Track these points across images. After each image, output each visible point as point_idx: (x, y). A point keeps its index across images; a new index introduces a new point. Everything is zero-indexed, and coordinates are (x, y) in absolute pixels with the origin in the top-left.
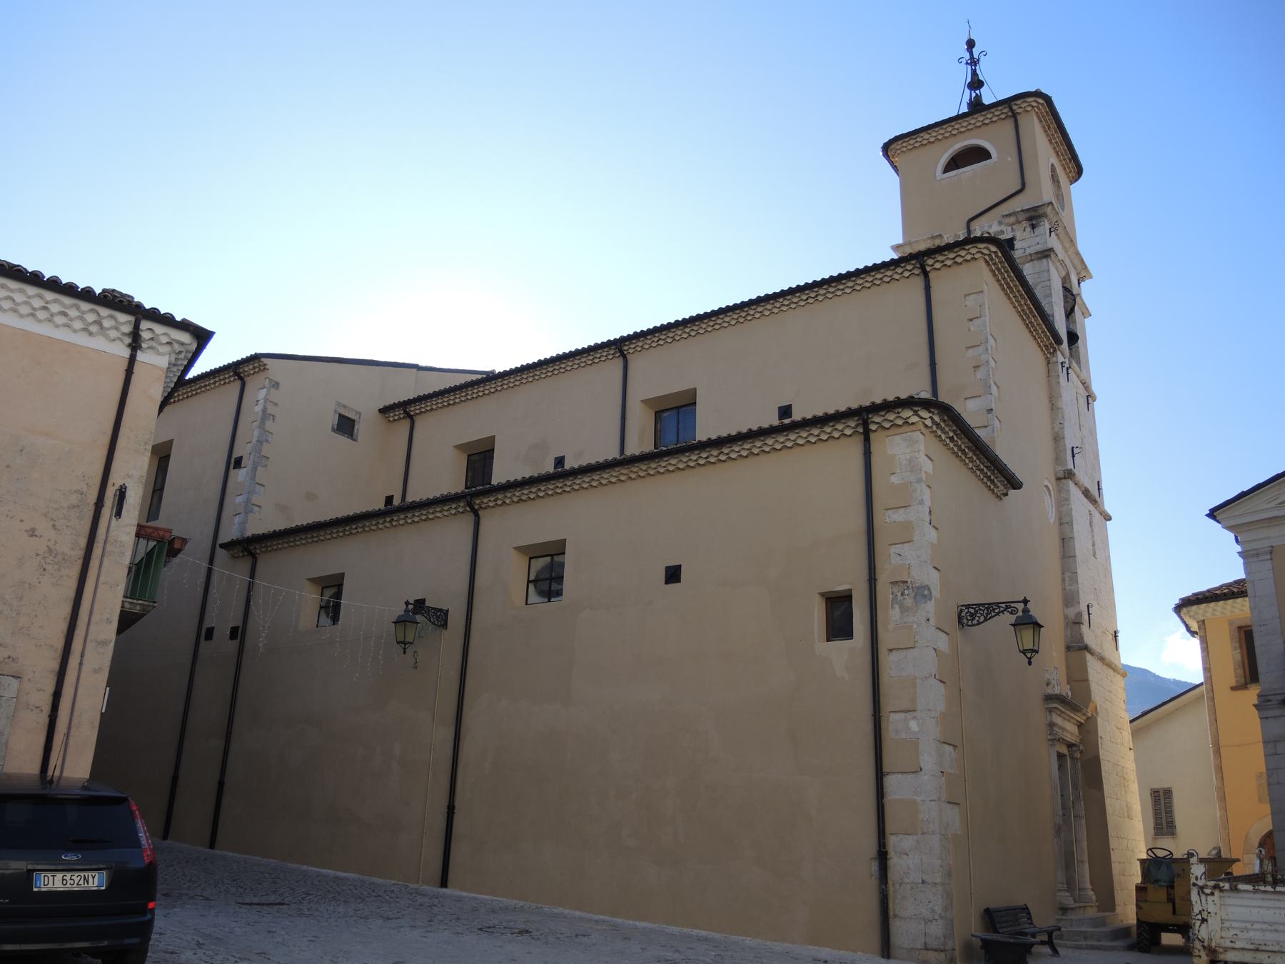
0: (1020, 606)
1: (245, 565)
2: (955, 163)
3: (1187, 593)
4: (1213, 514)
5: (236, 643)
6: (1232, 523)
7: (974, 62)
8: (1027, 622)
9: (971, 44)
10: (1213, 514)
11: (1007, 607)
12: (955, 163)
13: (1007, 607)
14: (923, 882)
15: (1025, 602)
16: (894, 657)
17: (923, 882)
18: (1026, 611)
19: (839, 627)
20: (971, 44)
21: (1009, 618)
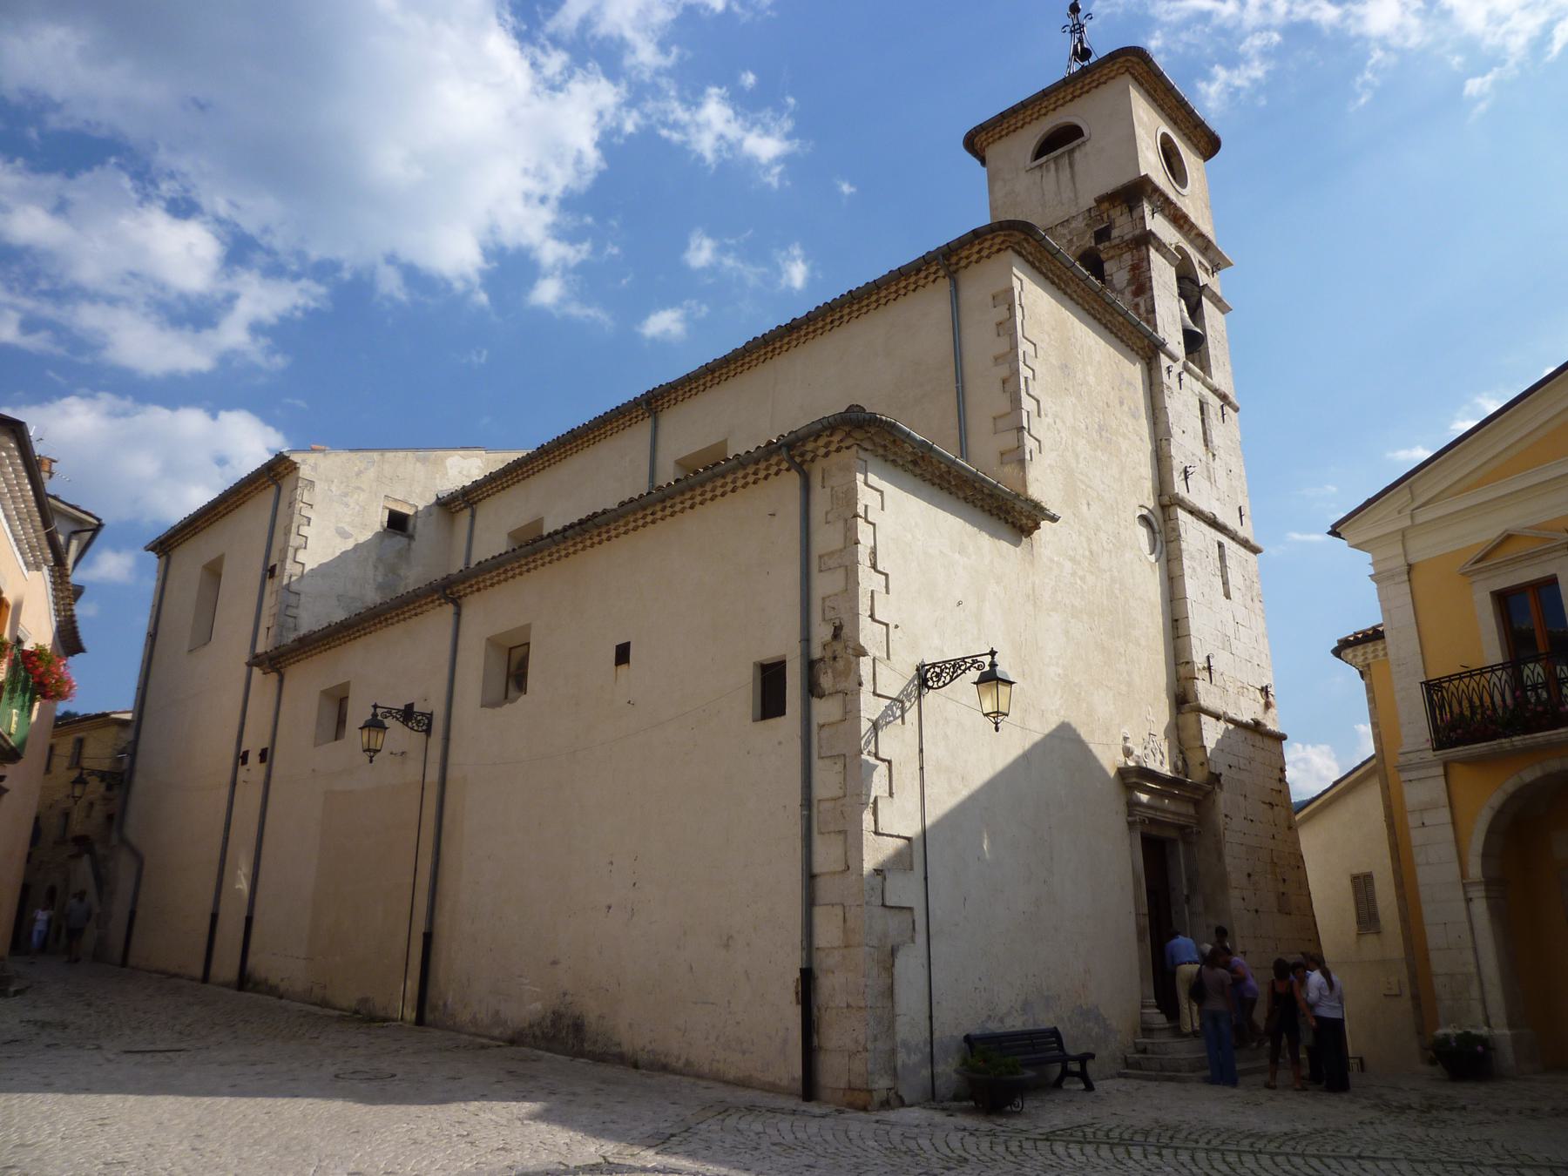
0: (987, 660)
1: (274, 677)
2: (1047, 146)
3: (1347, 632)
4: (1335, 532)
5: (264, 766)
6: (1357, 541)
7: (1078, 29)
8: (990, 678)
9: (1075, 9)
10: (1335, 532)
11: (974, 662)
12: (1047, 146)
13: (974, 662)
14: (848, 1006)
15: (993, 653)
16: (826, 733)
17: (848, 1006)
18: (993, 665)
19: (771, 702)
20: (1075, 9)
21: (974, 674)
